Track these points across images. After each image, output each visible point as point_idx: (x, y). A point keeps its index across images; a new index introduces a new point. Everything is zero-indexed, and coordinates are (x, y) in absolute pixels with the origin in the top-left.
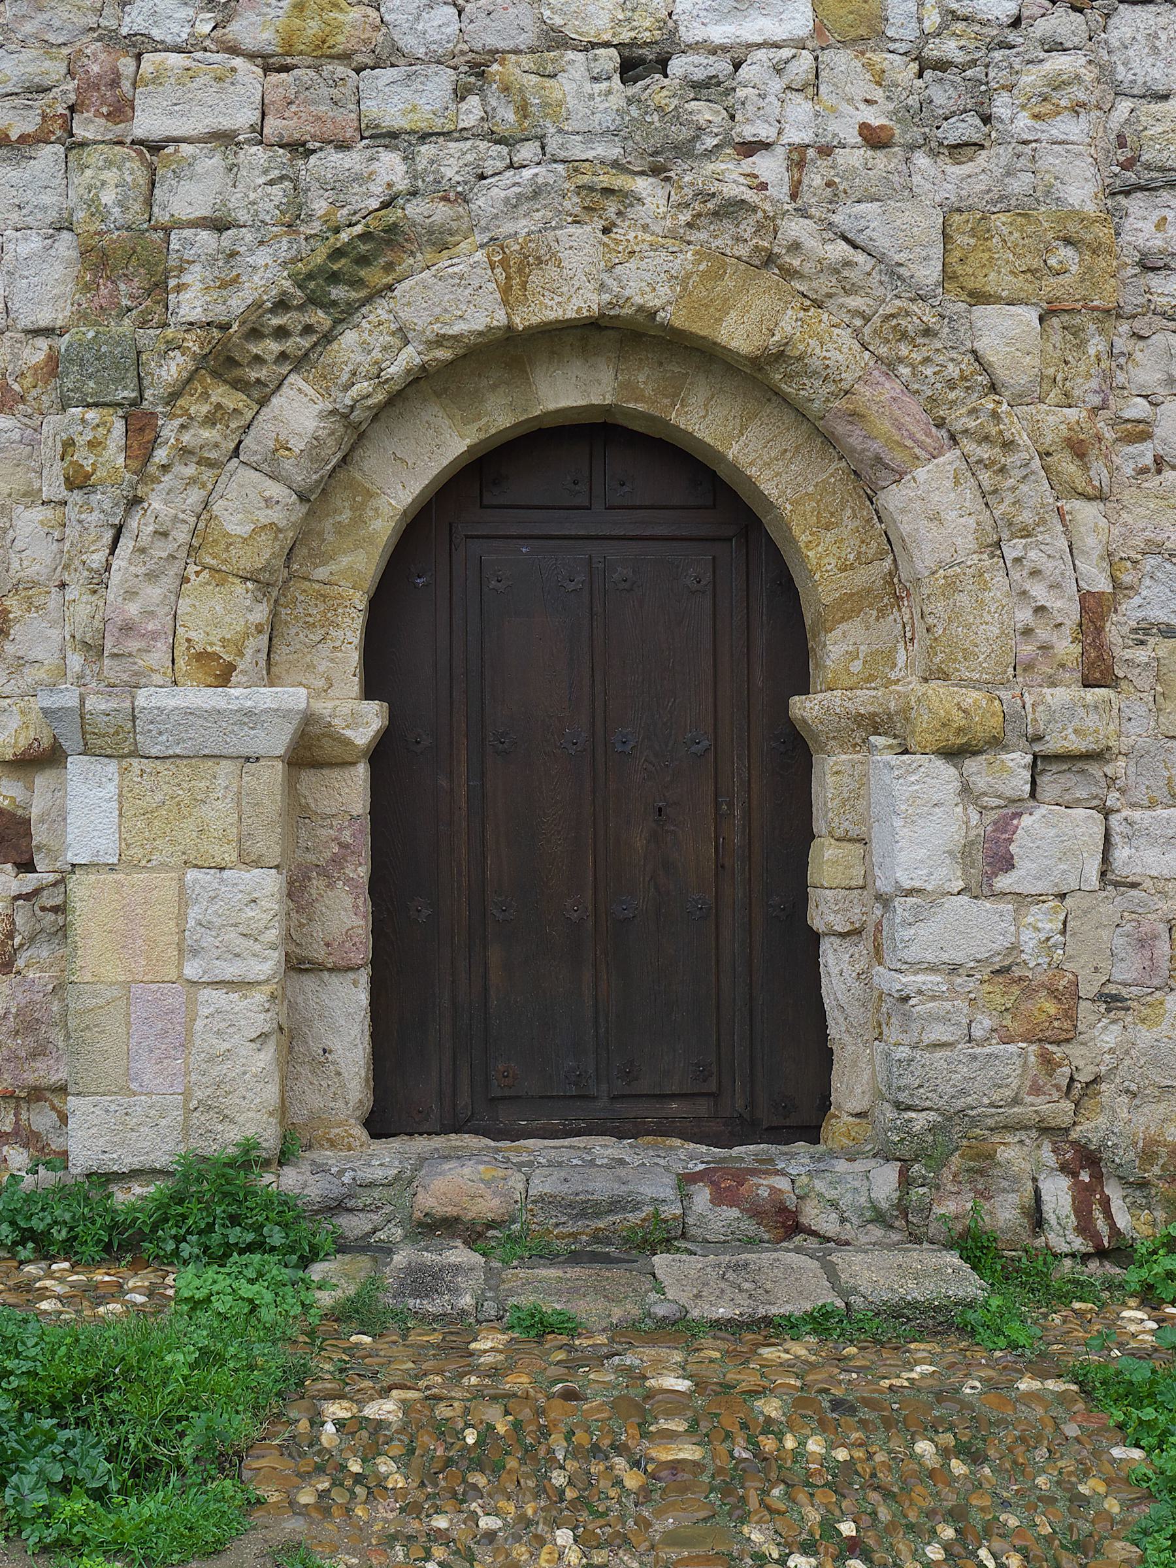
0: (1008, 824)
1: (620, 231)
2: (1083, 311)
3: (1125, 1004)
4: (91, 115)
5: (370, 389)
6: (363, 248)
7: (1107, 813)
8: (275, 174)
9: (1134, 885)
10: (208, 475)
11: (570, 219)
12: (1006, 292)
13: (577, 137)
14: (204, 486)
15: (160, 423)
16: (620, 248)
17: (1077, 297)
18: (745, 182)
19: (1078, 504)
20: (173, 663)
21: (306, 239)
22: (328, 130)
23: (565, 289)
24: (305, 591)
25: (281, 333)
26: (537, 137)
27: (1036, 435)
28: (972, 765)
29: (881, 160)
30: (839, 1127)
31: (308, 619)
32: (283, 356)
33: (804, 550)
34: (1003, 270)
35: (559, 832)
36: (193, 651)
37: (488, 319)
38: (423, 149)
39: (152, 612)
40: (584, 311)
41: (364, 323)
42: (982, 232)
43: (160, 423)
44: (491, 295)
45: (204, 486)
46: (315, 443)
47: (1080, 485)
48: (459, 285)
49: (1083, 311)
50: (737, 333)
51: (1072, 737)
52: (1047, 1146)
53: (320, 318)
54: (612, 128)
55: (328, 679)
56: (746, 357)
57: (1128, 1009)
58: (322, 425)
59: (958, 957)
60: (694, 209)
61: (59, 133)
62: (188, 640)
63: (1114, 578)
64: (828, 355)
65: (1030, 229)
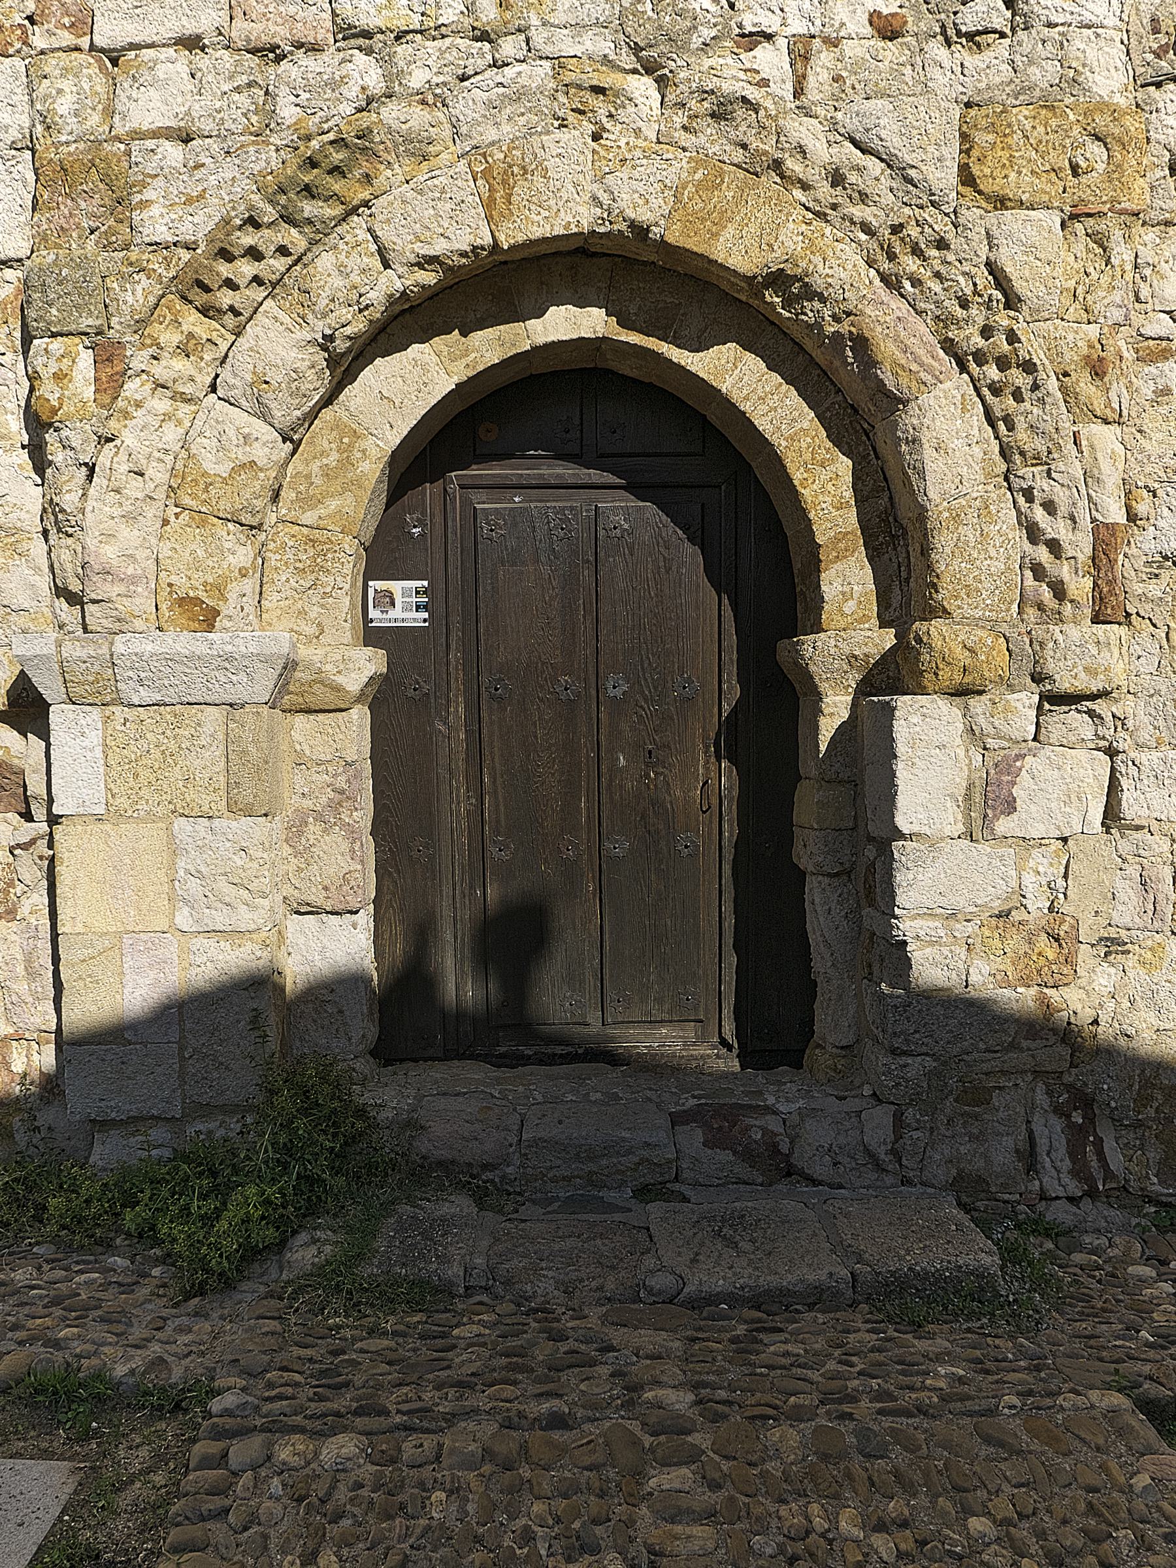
0: (1011, 766)
1: (611, 137)
2: (1110, 214)
3: (1126, 948)
4: (51, 26)
5: (349, 316)
6: (337, 157)
7: (1111, 752)
8: (243, 79)
9: (1138, 828)
10: (185, 409)
11: (556, 124)
12: (1027, 195)
13: (565, 32)
14: (179, 423)
15: (128, 353)
16: (611, 156)
17: (1105, 198)
18: (745, 78)
19: (1098, 428)
20: (157, 609)
21: (277, 150)
22: (302, 32)
23: (552, 202)
24: (293, 536)
25: (254, 254)
26: (519, 30)
27: (1055, 353)
28: (978, 704)
29: (891, 51)
30: (820, 1058)
31: (298, 565)
32: (257, 280)
33: (799, 488)
34: (1024, 171)
35: (553, 774)
36: (175, 596)
37: (472, 236)
38: (399, 49)
39: (131, 556)
40: (573, 226)
41: (342, 246)
42: (1000, 128)
43: (128, 353)
44: (475, 213)
45: (179, 423)
46: (294, 375)
47: (1099, 407)
48: (439, 199)
49: (1110, 214)
50: (738, 250)
51: (1082, 675)
52: (1040, 1088)
53: (295, 238)
54: (602, 19)
55: (319, 624)
56: (745, 277)
57: (1129, 952)
58: (300, 356)
59: (960, 902)
60: (690, 109)
61: (18, 45)
62: (170, 585)
63: (1128, 508)
64: (830, 272)
65: (1054, 123)
